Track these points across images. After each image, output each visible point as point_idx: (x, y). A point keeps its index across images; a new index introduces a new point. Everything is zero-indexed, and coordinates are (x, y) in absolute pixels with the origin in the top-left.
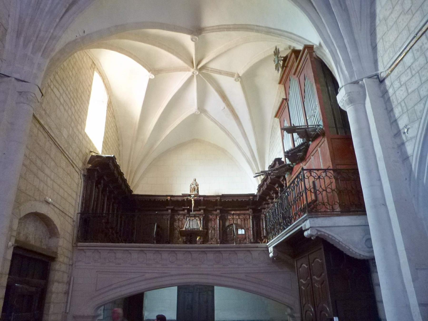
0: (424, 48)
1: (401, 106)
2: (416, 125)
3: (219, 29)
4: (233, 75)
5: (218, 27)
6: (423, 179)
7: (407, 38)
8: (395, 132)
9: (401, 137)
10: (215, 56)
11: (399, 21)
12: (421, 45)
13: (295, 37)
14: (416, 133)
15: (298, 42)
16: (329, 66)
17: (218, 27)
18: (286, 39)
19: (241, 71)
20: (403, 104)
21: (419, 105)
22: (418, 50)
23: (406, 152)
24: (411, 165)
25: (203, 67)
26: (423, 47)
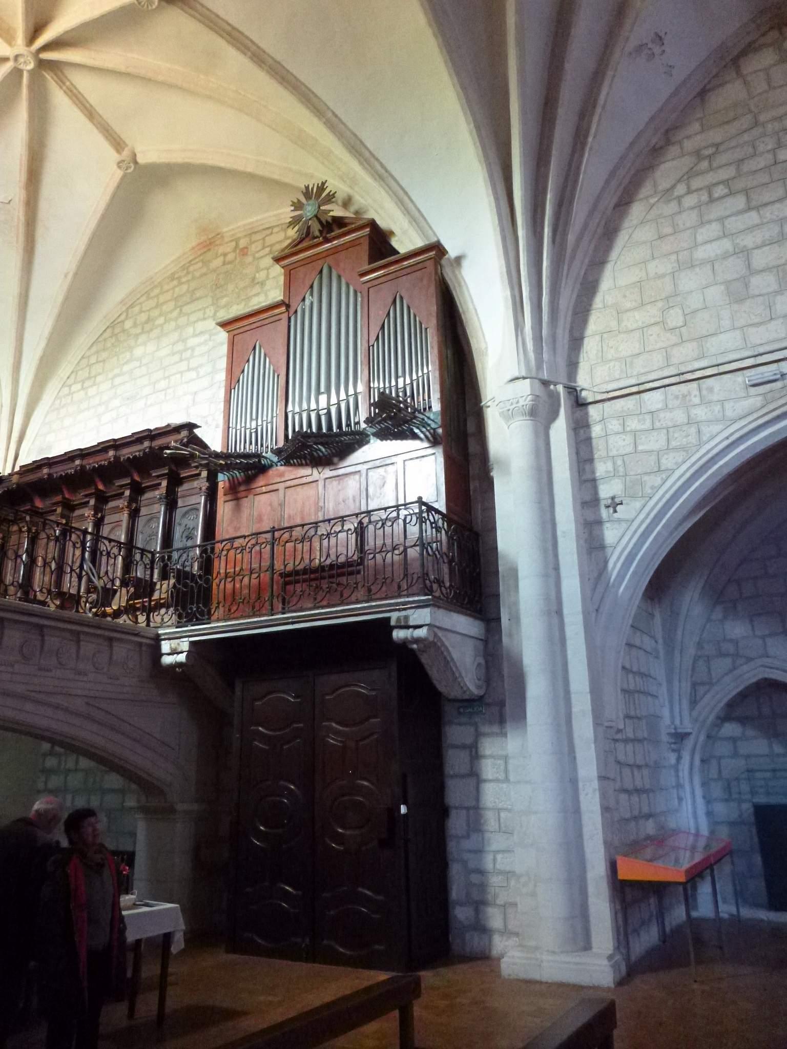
0: (690, 400)
1: (614, 463)
2: (638, 504)
3: (229, 34)
4: (119, 144)
5: (229, 28)
6: (619, 588)
7: (661, 369)
8: (588, 498)
9: (599, 510)
10: (122, 68)
11: (650, 332)
12: (686, 393)
13: (410, 205)
14: (633, 517)
15: (415, 221)
16: (464, 312)
17: (229, 28)
18: (387, 192)
19: (148, 155)
20: (619, 462)
21: (652, 477)
22: (677, 397)
23: (601, 538)
24: (606, 562)
25: (53, 66)
26: (688, 398)
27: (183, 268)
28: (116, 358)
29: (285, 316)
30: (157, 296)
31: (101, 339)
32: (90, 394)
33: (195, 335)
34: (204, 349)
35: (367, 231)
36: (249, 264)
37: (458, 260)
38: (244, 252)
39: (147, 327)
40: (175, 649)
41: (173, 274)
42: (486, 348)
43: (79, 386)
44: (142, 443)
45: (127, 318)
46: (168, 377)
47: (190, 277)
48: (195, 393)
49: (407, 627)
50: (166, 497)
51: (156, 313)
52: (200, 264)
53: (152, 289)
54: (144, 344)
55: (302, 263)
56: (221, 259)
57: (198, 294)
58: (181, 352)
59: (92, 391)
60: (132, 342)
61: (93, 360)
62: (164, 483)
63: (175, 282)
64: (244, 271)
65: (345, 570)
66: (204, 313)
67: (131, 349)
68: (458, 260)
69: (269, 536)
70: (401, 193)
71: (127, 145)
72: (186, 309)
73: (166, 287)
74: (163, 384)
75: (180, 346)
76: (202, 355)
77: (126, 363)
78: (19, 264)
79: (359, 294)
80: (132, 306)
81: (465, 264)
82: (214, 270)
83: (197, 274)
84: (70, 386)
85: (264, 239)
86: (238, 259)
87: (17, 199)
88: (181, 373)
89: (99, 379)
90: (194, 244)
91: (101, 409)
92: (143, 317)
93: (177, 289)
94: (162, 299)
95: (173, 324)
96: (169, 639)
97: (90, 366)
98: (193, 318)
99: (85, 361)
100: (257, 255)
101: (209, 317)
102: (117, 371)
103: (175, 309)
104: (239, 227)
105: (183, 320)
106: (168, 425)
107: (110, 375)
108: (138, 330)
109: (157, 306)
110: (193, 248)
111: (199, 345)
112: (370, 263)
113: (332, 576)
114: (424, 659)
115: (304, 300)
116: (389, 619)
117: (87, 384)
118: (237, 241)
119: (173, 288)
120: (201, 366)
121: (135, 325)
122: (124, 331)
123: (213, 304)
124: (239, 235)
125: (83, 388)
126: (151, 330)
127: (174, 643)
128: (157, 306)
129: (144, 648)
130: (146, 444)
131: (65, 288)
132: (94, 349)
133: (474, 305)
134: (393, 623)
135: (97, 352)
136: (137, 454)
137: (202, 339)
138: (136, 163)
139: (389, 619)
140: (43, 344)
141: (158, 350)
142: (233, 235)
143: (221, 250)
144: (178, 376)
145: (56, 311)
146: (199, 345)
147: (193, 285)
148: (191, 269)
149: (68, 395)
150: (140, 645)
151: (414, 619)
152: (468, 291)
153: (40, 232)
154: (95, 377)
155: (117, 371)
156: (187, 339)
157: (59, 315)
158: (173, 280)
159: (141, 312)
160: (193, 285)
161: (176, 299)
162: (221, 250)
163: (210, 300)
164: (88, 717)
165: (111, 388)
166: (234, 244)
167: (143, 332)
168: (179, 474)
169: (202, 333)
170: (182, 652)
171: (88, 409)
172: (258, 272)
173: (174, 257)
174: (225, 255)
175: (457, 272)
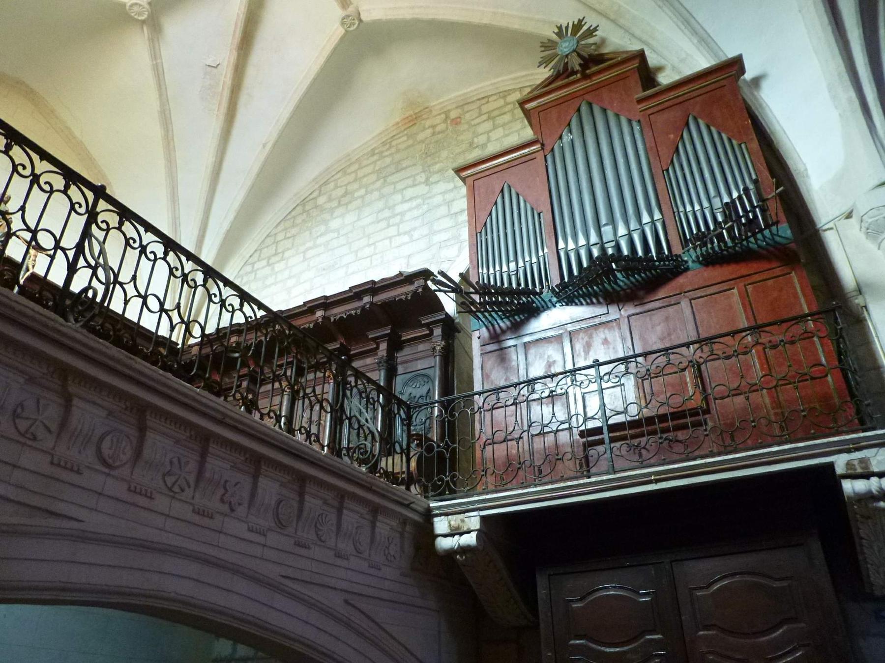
15: (703, 40)
27: (384, 144)
28: (308, 233)
29: (540, 156)
30: (355, 171)
31: (289, 217)
32: (277, 269)
33: (404, 201)
34: (416, 213)
35: (635, 64)
36: (464, 131)
37: (756, 82)
38: (456, 122)
39: (344, 200)
40: (458, 528)
41: (373, 150)
42: (806, 170)
43: (264, 263)
44: (361, 299)
45: (320, 195)
46: (374, 244)
47: (393, 150)
48: (409, 256)
49: (867, 476)
50: (387, 362)
51: (356, 186)
52: (405, 138)
53: (349, 166)
54: (343, 215)
55: (554, 104)
56: (430, 131)
57: (404, 165)
58: (387, 219)
59: (279, 267)
60: (326, 216)
61: (280, 237)
62: (383, 346)
63: (376, 157)
64: (460, 138)
65: (689, 420)
66: (415, 180)
67: (325, 222)
68: (756, 82)
69: (592, 371)
70: (688, 15)
71: (351, 3)
72: (390, 179)
73: (365, 163)
74: (368, 251)
75: (387, 213)
76: (416, 218)
77: (321, 236)
78: (218, 131)
79: (635, 124)
80: (326, 183)
81: (765, 85)
82: (422, 141)
83: (402, 147)
84: (253, 264)
85: (479, 108)
86: (450, 128)
87: (225, 64)
88: (390, 238)
89: (287, 254)
90: (398, 120)
91: (290, 283)
92: (340, 192)
93: (379, 163)
94: (360, 173)
95: (376, 194)
96: (447, 514)
97: (277, 243)
98: (400, 186)
99: (269, 241)
100: (473, 123)
101: (420, 183)
102: (308, 245)
103: (378, 180)
104: (450, 99)
105: (387, 190)
106: (401, 274)
107: (302, 249)
108: (334, 204)
109: (355, 180)
110: (398, 123)
111: (410, 210)
112: (644, 91)
113: (666, 430)
114: (864, 531)
115: (561, 138)
116: (831, 465)
117: (273, 260)
118: (447, 113)
119: (375, 162)
120: (415, 229)
121: (330, 200)
122: (316, 207)
123: (424, 171)
124: (449, 108)
125: (269, 264)
126: (350, 202)
127: (455, 520)
128: (355, 180)
129: (408, 528)
130: (367, 299)
131: (262, 158)
132: (280, 228)
133: (782, 128)
134: (840, 469)
135: (286, 229)
136: (353, 312)
137: (414, 203)
138: (360, 21)
139: (831, 465)
140: (231, 217)
141: (358, 220)
142: (442, 108)
143: (428, 123)
144: (387, 241)
145: (249, 183)
146: (410, 210)
147: (397, 157)
148: (394, 143)
149: (251, 272)
150: (405, 521)
151: (879, 462)
152: (771, 111)
153: (243, 99)
154: (283, 252)
155: (308, 245)
156: (394, 205)
157: (252, 187)
158: (373, 155)
159: (336, 187)
160: (397, 157)
161: (379, 171)
162: (428, 123)
163: (420, 168)
164: (348, 625)
165: (304, 261)
166: (443, 116)
167: (340, 205)
168: (400, 337)
169: (411, 199)
170: (469, 532)
171: (275, 284)
172: (477, 137)
173: (375, 134)
174: (433, 127)
175: (756, 93)
